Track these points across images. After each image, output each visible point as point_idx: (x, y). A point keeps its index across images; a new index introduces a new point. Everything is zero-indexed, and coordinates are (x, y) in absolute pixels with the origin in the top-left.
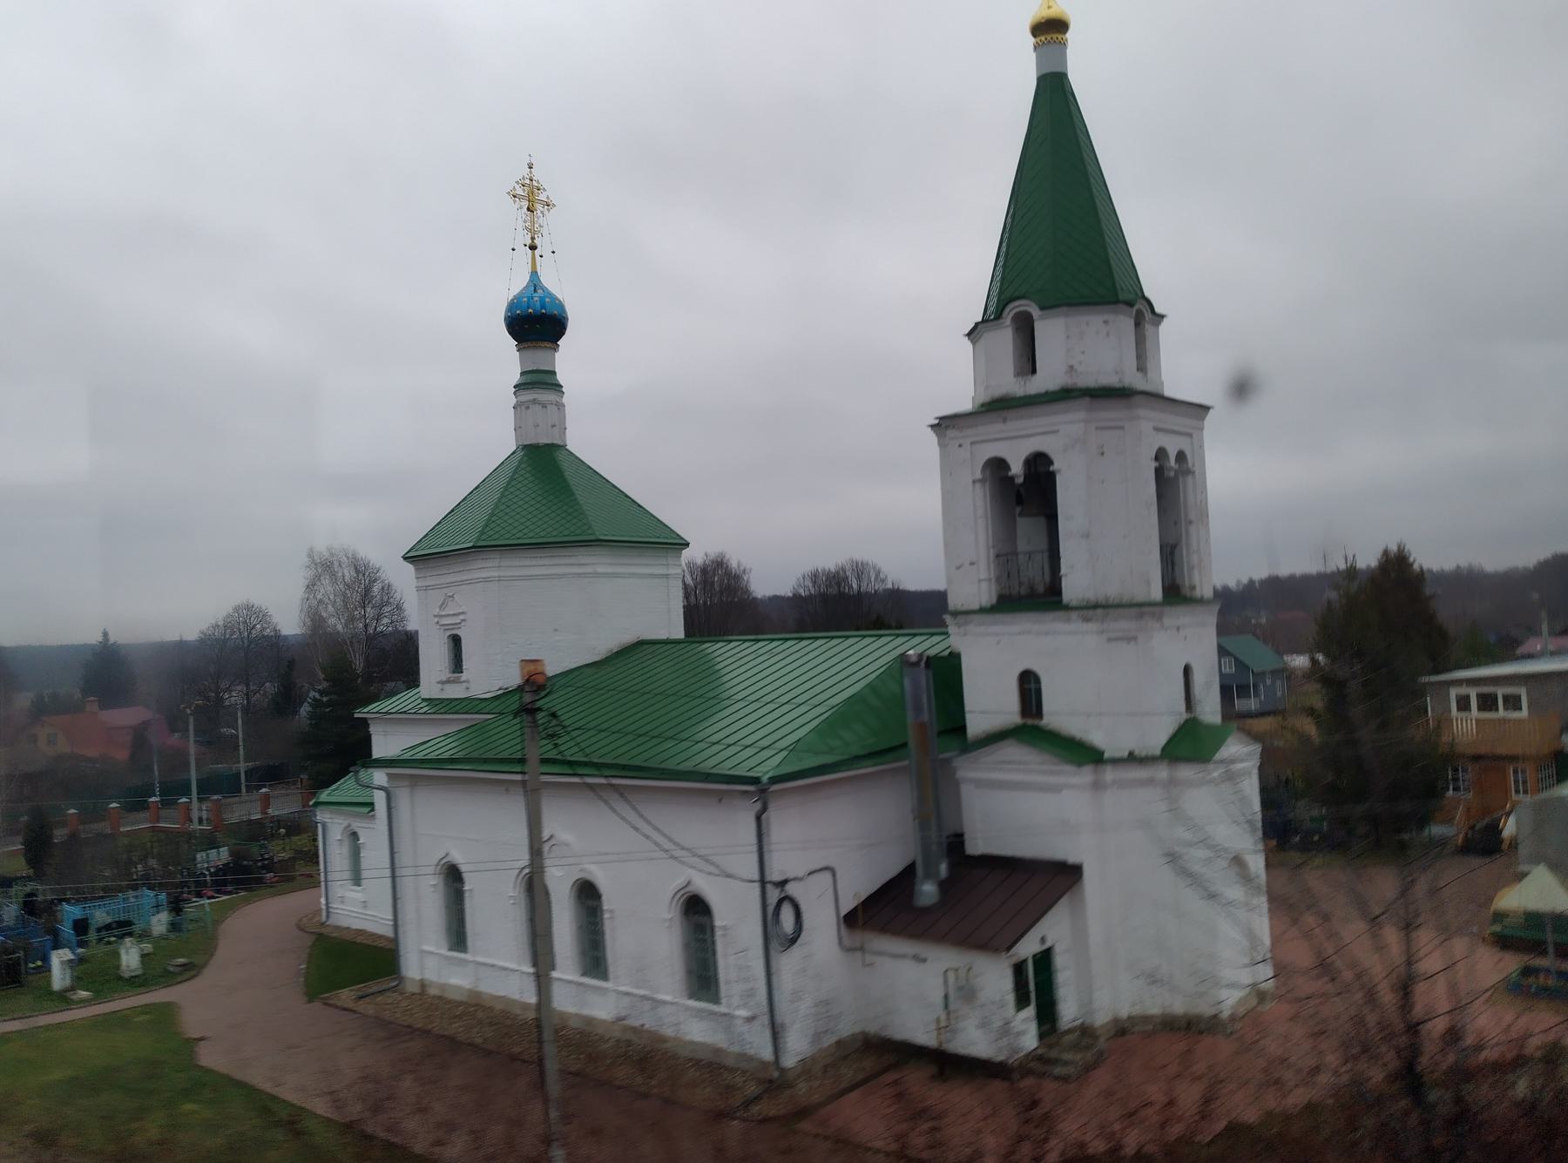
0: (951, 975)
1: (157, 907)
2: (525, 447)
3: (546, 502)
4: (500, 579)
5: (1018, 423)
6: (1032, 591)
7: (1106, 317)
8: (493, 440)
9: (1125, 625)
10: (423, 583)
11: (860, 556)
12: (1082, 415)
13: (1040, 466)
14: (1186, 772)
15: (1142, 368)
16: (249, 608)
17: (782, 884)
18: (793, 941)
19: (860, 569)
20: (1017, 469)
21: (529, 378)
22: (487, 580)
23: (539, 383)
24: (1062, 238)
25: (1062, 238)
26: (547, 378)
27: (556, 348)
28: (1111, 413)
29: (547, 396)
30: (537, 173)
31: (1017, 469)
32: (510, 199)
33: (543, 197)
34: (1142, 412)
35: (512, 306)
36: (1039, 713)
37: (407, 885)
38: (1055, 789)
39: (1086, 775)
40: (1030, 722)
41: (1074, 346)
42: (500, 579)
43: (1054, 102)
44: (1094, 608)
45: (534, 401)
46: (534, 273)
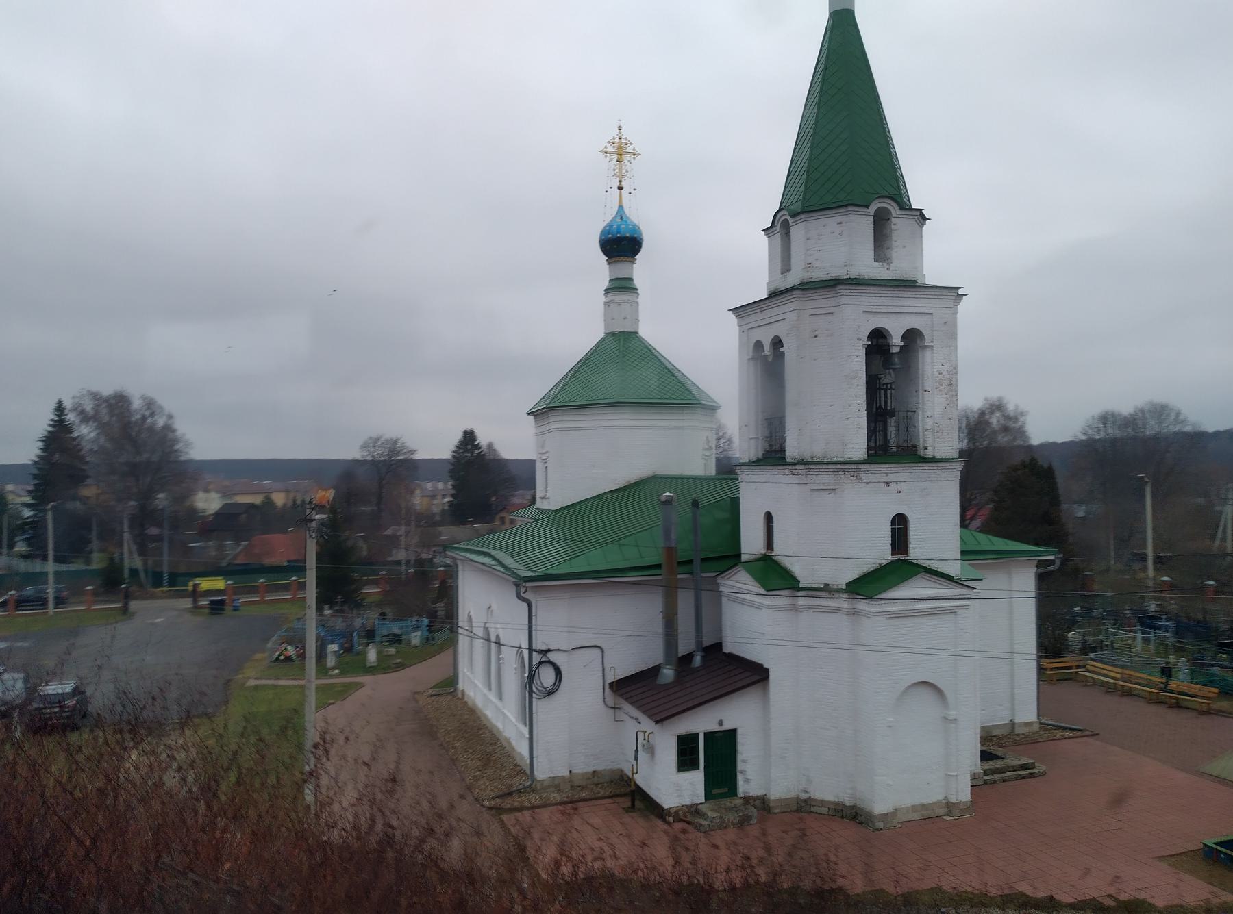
0: (641, 735)
1: (417, 628)
2: (613, 334)
7: (839, 219)
8: (585, 333)
9: (826, 479)
10: (540, 430)
11: (1160, 397)
13: (912, 337)
14: (862, 605)
16: (394, 447)
17: (545, 652)
18: (550, 693)
19: (1160, 411)
21: (617, 284)
23: (622, 286)
24: (845, 153)
25: (845, 153)
26: (624, 284)
27: (633, 262)
30: (625, 133)
32: (602, 156)
33: (630, 149)
34: (844, 300)
35: (603, 233)
38: (758, 607)
40: (898, 557)
41: (841, 243)
44: (805, 463)
46: (621, 207)
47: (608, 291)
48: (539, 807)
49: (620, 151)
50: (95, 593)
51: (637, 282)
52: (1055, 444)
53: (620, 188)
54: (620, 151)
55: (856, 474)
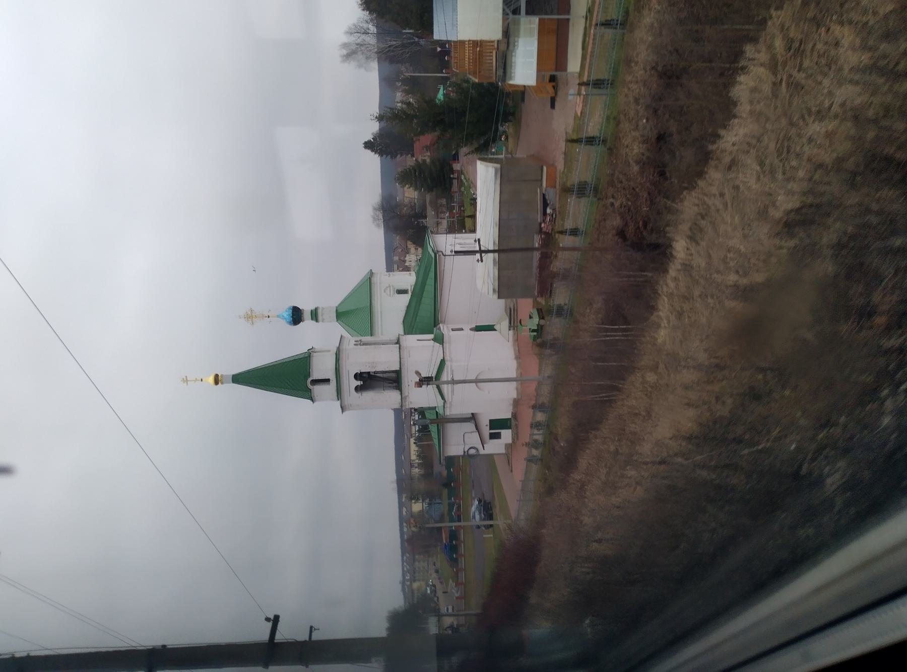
6: (394, 380)
13: (357, 376)
15: (329, 351)
20: (359, 383)
28: (343, 356)
29: (320, 312)
31: (359, 383)
39: (448, 363)
43: (238, 379)
47: (317, 321)
48: (546, 259)
49: (250, 317)
50: (456, 554)
51: (313, 308)
55: (406, 397)
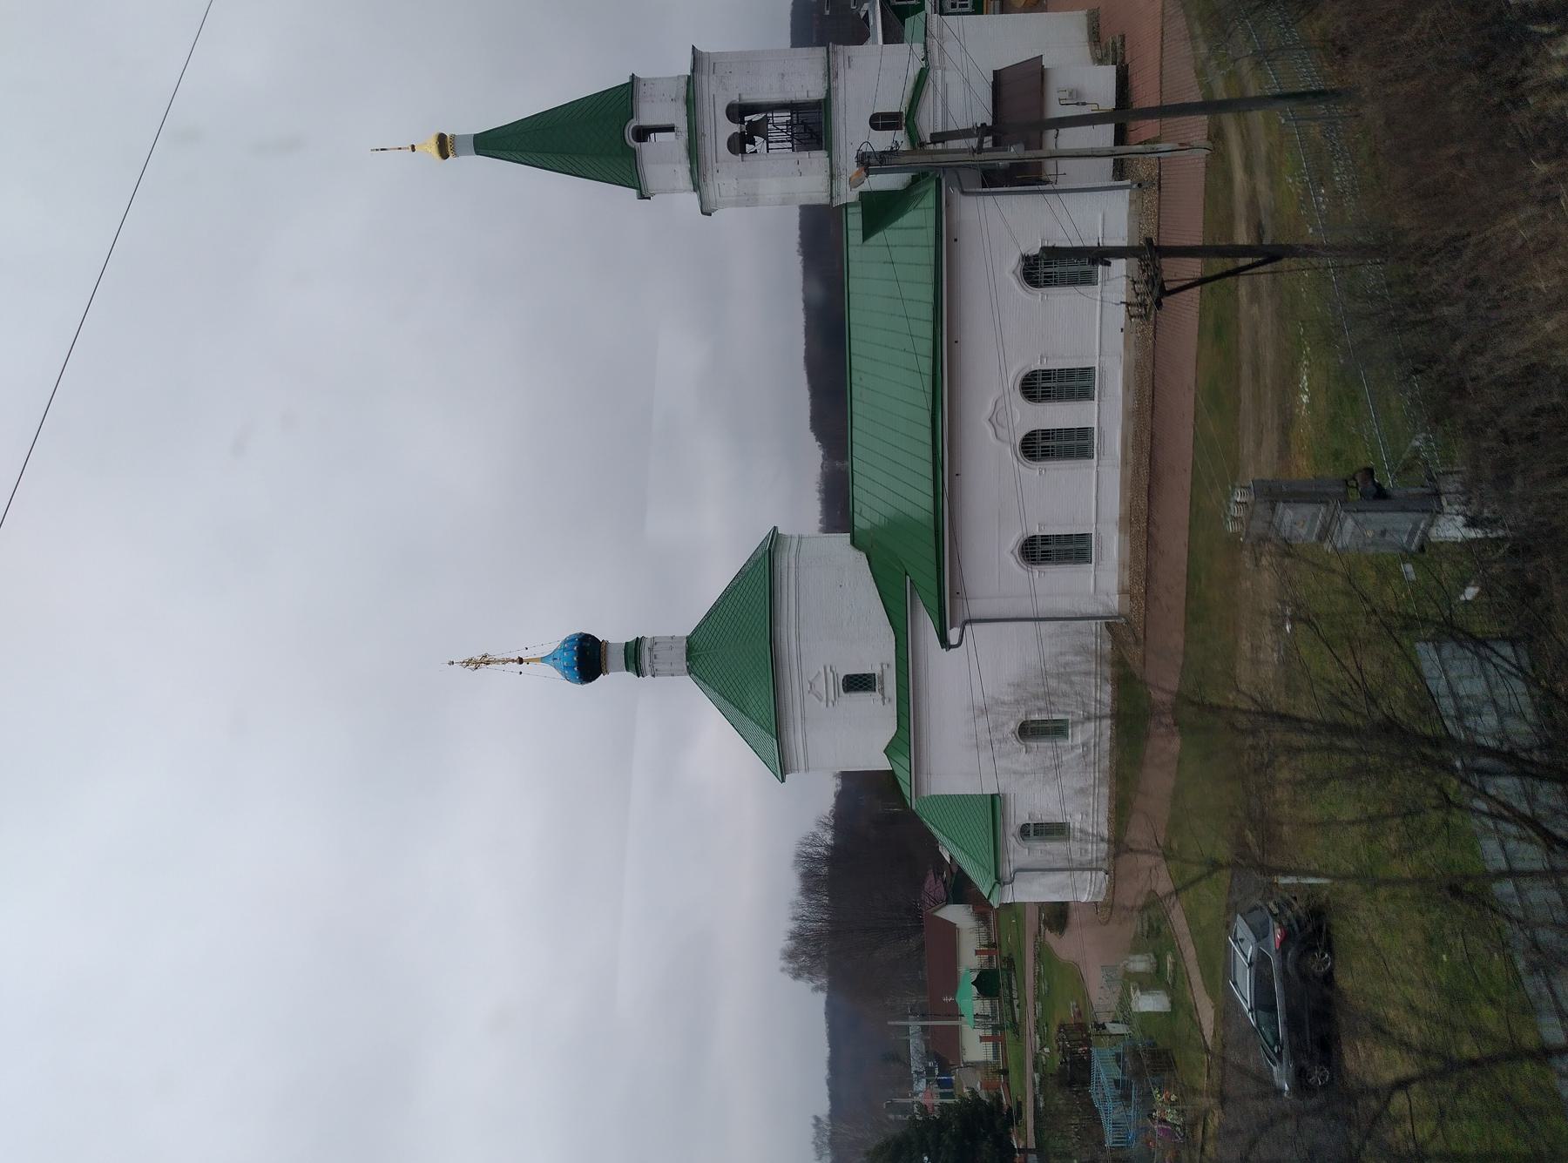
3: (739, 652)
4: (798, 627)
5: (707, 126)
12: (705, 78)
22: (798, 637)
23: (634, 657)
36: (897, 115)
37: (1045, 606)
42: (798, 627)
43: (492, 144)
45: (651, 650)
46: (543, 659)
47: (639, 672)
52: (834, 1064)
53: (521, 661)
54: (589, 138)
